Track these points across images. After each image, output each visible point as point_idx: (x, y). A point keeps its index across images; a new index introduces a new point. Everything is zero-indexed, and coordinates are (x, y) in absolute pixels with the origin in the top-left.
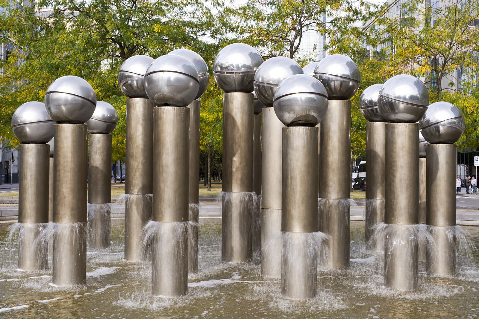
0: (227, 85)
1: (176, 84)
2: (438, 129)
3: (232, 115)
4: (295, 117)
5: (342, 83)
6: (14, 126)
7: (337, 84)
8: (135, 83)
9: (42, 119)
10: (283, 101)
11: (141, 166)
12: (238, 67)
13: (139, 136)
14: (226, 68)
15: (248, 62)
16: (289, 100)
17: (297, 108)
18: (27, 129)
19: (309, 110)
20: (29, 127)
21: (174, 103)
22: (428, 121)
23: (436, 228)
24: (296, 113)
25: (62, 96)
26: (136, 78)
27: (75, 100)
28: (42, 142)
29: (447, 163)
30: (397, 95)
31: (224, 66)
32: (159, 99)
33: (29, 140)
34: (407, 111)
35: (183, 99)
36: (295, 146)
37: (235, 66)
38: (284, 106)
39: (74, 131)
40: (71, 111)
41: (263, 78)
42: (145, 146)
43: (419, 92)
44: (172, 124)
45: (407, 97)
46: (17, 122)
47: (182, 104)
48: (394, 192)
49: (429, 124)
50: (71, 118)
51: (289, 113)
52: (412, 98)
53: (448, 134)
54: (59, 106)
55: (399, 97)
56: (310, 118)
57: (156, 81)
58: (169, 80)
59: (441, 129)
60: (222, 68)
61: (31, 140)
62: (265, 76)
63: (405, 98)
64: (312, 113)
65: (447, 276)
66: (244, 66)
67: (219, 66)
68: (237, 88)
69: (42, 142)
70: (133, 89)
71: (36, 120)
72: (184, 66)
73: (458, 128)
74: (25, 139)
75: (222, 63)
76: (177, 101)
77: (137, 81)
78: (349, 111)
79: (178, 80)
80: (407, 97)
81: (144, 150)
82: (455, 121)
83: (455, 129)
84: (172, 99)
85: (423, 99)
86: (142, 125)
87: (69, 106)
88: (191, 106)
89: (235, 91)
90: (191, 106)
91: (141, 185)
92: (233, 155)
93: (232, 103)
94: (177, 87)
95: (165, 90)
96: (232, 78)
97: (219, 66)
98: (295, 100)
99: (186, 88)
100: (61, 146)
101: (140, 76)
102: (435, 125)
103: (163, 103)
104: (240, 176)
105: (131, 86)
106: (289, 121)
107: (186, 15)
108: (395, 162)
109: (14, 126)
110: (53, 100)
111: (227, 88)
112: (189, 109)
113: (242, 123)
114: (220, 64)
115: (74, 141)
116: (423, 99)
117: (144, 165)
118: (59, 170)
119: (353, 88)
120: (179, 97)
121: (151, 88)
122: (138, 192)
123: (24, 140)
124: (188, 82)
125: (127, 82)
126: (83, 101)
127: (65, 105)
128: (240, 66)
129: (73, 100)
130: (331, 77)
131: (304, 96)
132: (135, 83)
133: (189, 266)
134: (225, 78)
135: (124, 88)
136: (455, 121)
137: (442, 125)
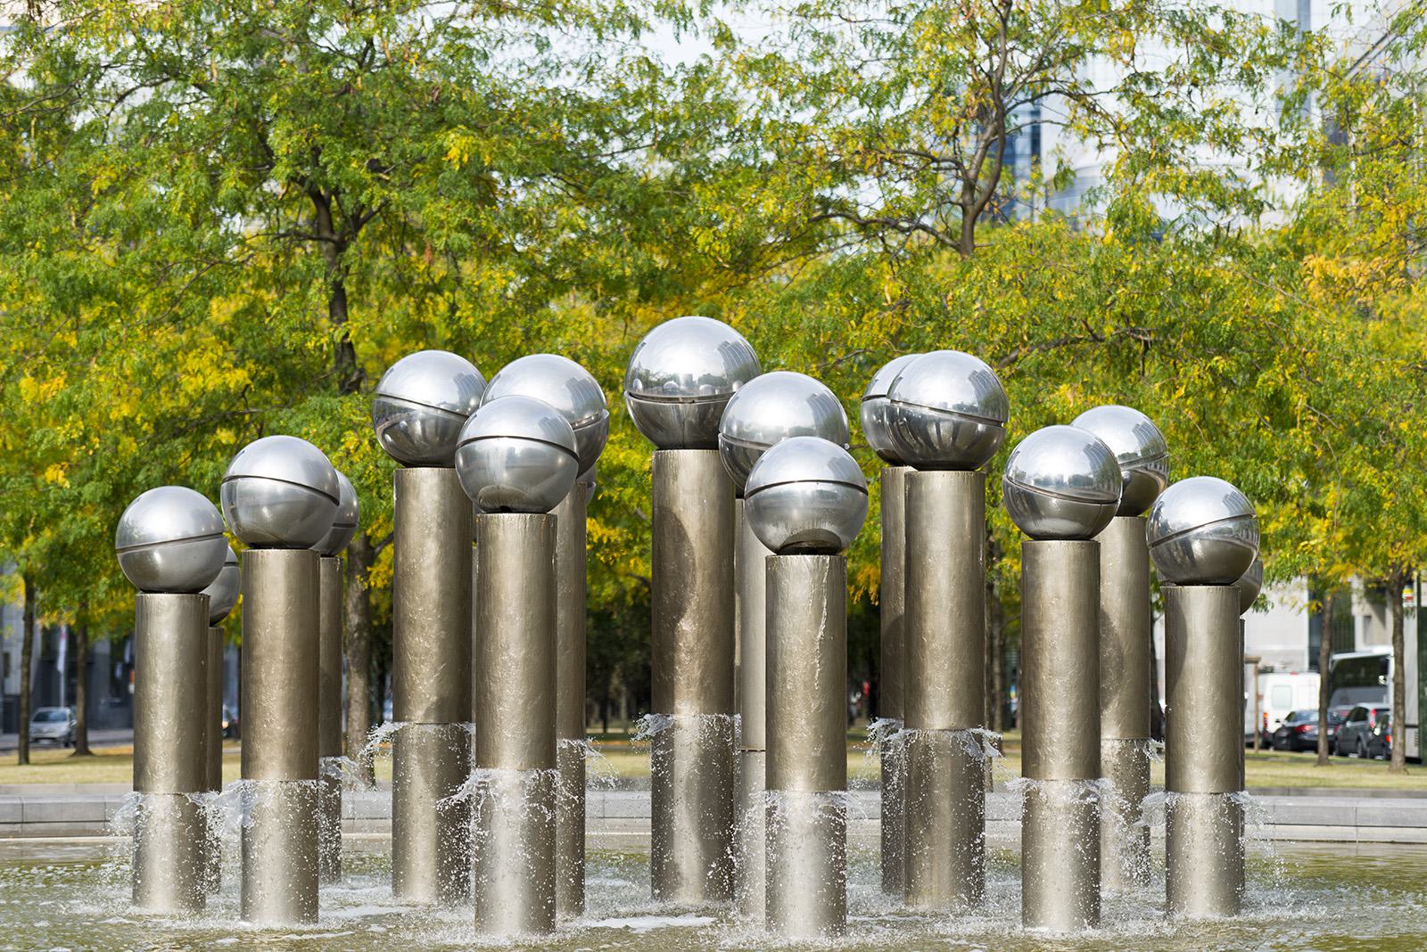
0: (661, 429)
1: (526, 464)
2: (1187, 547)
3: (675, 510)
4: (788, 534)
5: (957, 427)
6: (123, 550)
7: (946, 429)
8: (418, 428)
9: (193, 533)
10: (764, 498)
11: (434, 648)
12: (690, 383)
13: (429, 567)
14: (660, 383)
15: (718, 369)
16: (778, 496)
17: (796, 514)
18: (158, 557)
19: (819, 519)
20: (163, 554)
21: (522, 506)
22: (1165, 526)
23: (1188, 797)
24: (790, 526)
25: (265, 486)
26: (421, 415)
27: (293, 493)
28: (190, 588)
29: (1211, 633)
30: (1043, 474)
31: (653, 379)
32: (489, 498)
33: (162, 584)
34: (1069, 514)
35: (542, 497)
36: (791, 599)
37: (682, 381)
38: (765, 508)
39: (289, 567)
40: (284, 520)
41: (740, 425)
42: (444, 593)
43: (1093, 467)
44: (518, 551)
45: (1066, 480)
46: (131, 539)
47: (540, 507)
48: (1036, 702)
49: (1165, 536)
50: (285, 536)
51: (776, 525)
52: (1076, 481)
53: (1212, 558)
54: (256, 507)
55: (1046, 482)
56: (822, 537)
57: (481, 456)
58: (511, 455)
59: (1197, 548)
60: (647, 384)
61: (168, 584)
62: (746, 423)
63: (1059, 483)
64: (827, 527)
65: (1216, 917)
66: (707, 379)
67: (640, 377)
68: (688, 439)
69: (190, 588)
70: (412, 442)
71: (179, 535)
72: (545, 423)
73: (1238, 542)
74: (148, 581)
75: (648, 372)
76: (530, 502)
77: (423, 422)
78: (980, 503)
79: (530, 454)
80: (1066, 480)
81: (442, 606)
82: (1230, 525)
83: (1230, 547)
84: (518, 497)
85: (1103, 483)
86: (437, 536)
87: (280, 507)
88: (561, 510)
89: (684, 447)
90: (561, 510)
91: (434, 699)
92: (679, 612)
93: (675, 477)
94: (530, 471)
95: (503, 478)
96: (673, 416)
97: (640, 377)
98: (789, 495)
99: (549, 471)
100: (261, 600)
101: (431, 410)
102: (1181, 537)
103: (497, 506)
104: (697, 674)
105: (407, 433)
106: (778, 543)
107: (563, 72)
108: (1039, 631)
109: (123, 550)
110: (245, 494)
111: (661, 436)
112: (555, 517)
113: (702, 531)
114: (642, 371)
115: (290, 591)
116: (1103, 483)
117: (443, 644)
118: (259, 658)
119: (987, 436)
120: (532, 492)
121: (470, 472)
122: (426, 715)
123: (149, 584)
124: (553, 461)
125: (397, 423)
126: (310, 496)
127: (270, 506)
128: (695, 379)
129: (289, 494)
130: (926, 412)
131: (811, 489)
132: (418, 428)
133: (560, 893)
134: (657, 410)
135: (388, 437)
136: (1230, 525)
137: (1198, 536)
